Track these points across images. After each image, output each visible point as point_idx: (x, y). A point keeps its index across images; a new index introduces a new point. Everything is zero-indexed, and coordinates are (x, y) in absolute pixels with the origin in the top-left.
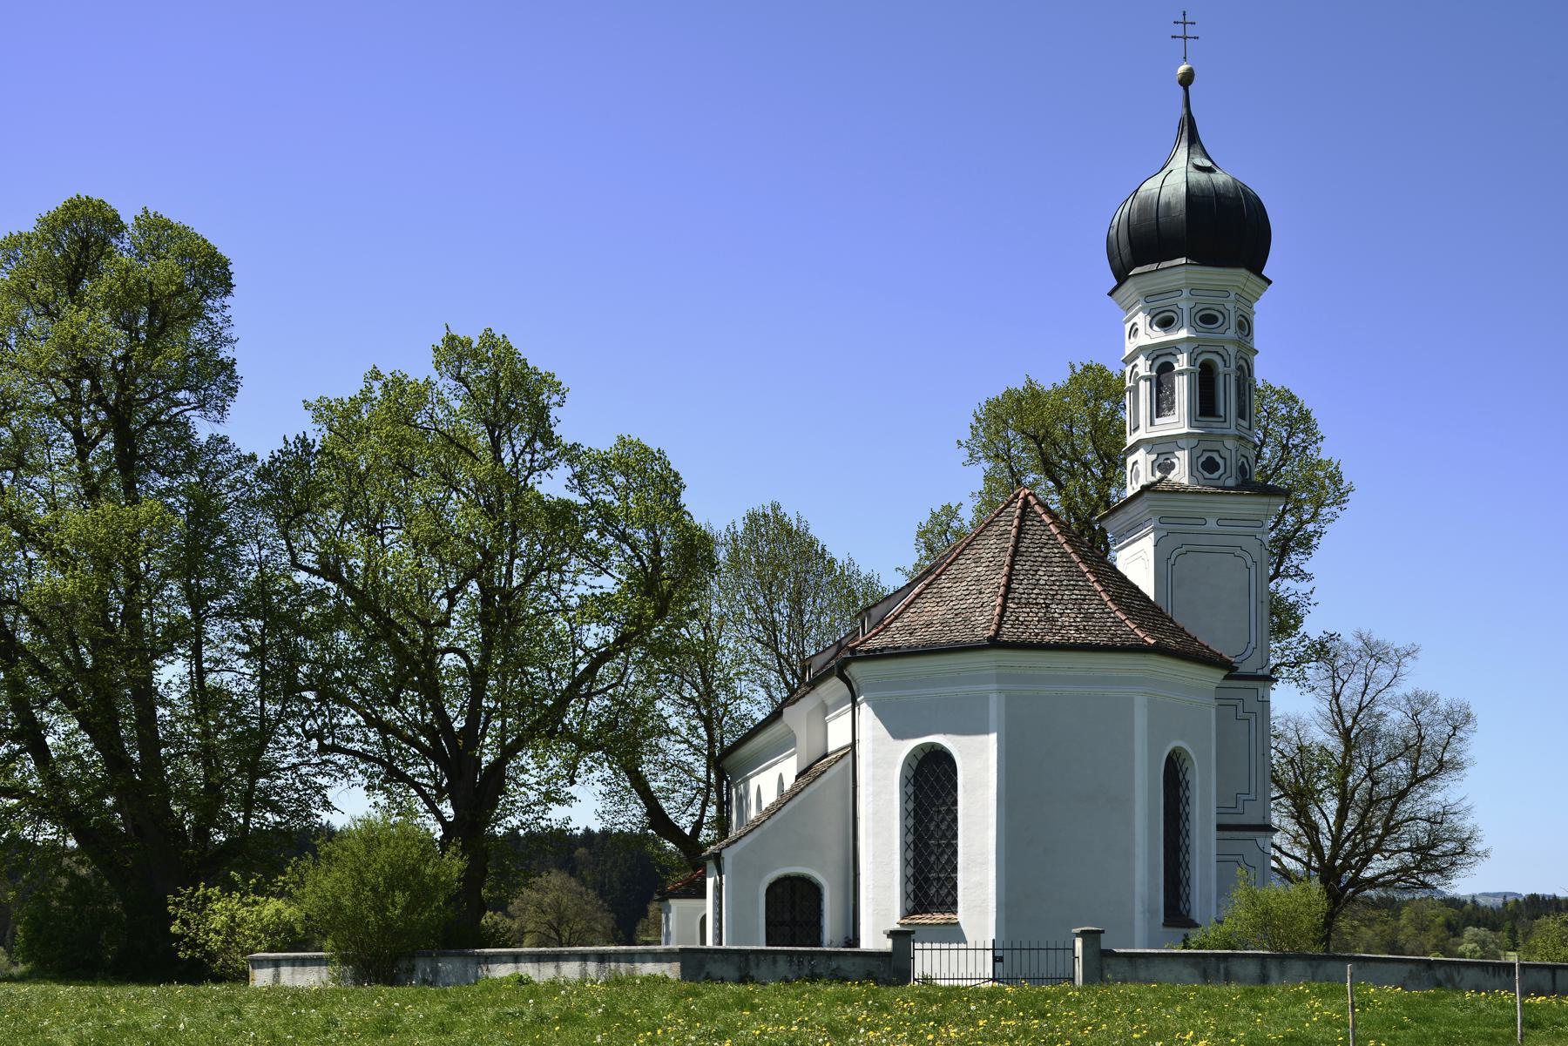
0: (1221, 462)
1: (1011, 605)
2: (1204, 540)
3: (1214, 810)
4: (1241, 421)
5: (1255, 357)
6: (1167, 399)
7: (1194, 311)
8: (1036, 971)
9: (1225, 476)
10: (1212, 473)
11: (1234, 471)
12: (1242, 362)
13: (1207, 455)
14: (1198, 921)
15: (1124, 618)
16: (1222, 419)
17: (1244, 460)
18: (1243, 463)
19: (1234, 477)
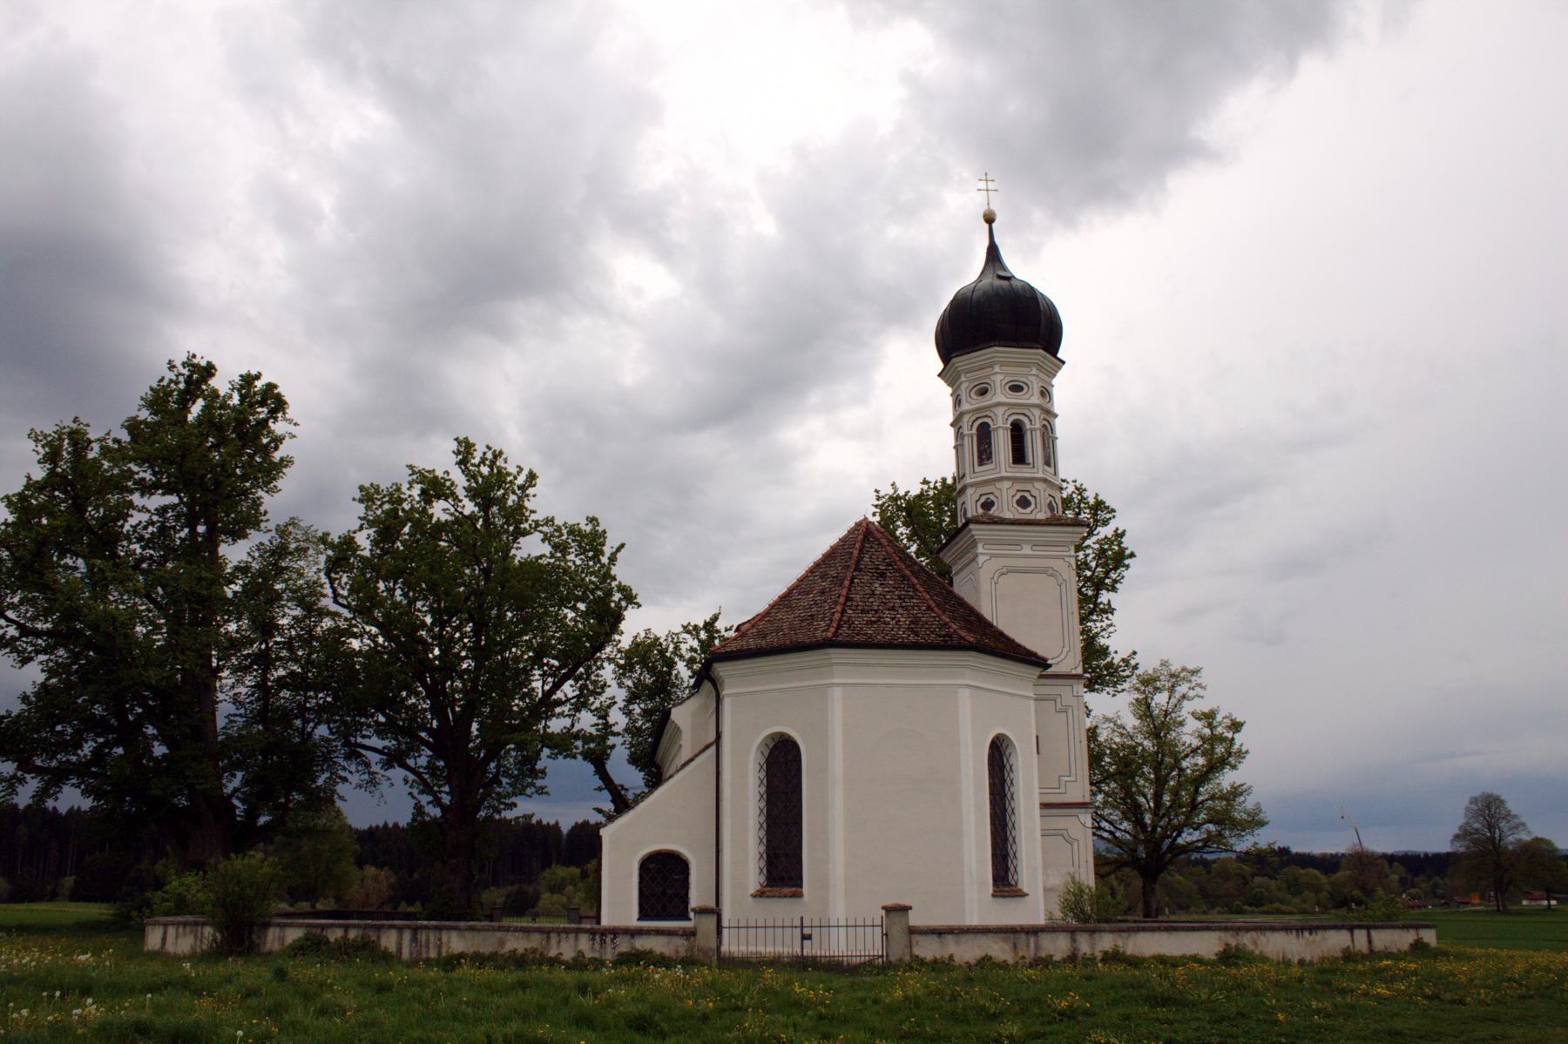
0: (1032, 500)
1: (849, 611)
2: (1021, 563)
3: (1037, 791)
4: (1046, 468)
5: (1057, 420)
6: (985, 450)
7: (1004, 383)
8: (845, 950)
9: (1037, 510)
10: (1022, 496)
11: (1043, 507)
12: (1046, 423)
13: (1020, 494)
14: (1026, 890)
15: (948, 620)
16: (1031, 466)
17: (1051, 498)
18: (1051, 501)
19: (1043, 511)
